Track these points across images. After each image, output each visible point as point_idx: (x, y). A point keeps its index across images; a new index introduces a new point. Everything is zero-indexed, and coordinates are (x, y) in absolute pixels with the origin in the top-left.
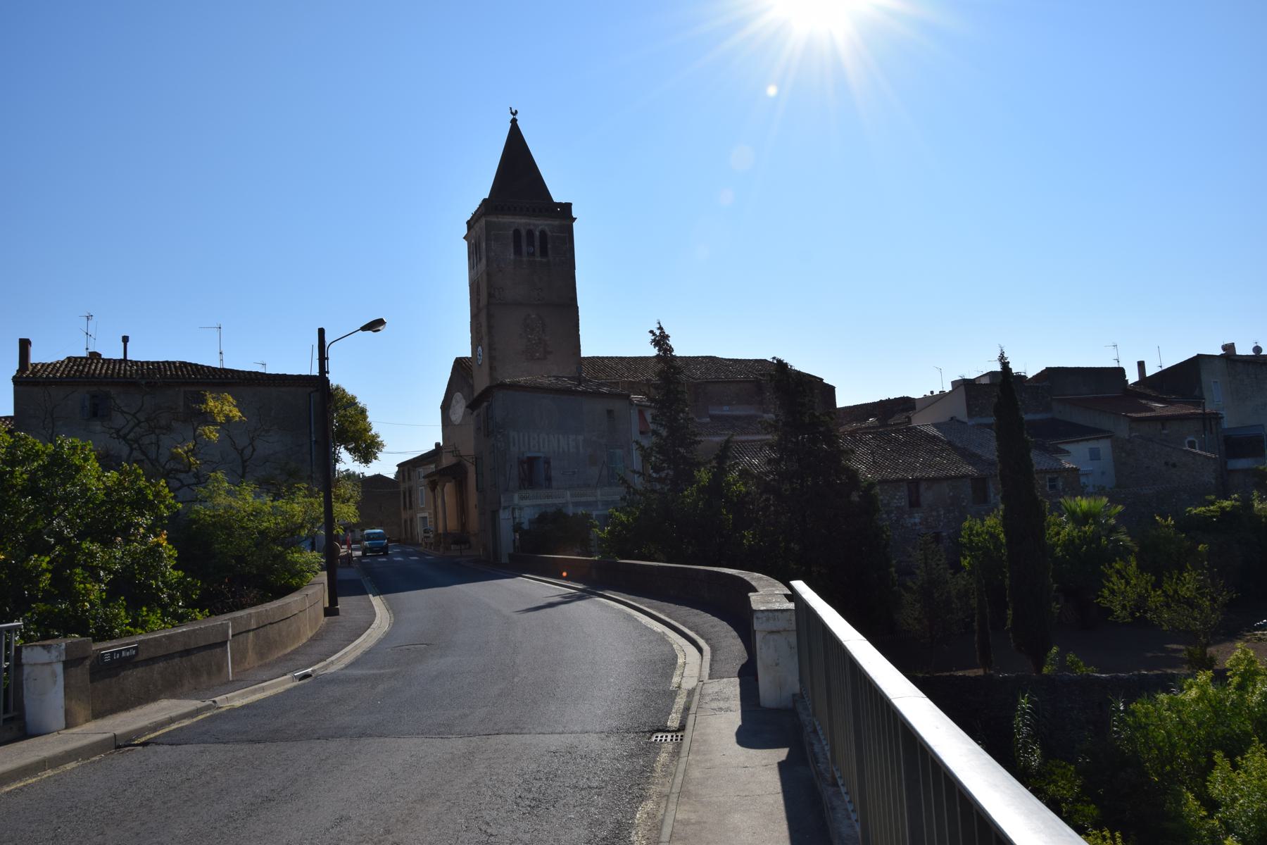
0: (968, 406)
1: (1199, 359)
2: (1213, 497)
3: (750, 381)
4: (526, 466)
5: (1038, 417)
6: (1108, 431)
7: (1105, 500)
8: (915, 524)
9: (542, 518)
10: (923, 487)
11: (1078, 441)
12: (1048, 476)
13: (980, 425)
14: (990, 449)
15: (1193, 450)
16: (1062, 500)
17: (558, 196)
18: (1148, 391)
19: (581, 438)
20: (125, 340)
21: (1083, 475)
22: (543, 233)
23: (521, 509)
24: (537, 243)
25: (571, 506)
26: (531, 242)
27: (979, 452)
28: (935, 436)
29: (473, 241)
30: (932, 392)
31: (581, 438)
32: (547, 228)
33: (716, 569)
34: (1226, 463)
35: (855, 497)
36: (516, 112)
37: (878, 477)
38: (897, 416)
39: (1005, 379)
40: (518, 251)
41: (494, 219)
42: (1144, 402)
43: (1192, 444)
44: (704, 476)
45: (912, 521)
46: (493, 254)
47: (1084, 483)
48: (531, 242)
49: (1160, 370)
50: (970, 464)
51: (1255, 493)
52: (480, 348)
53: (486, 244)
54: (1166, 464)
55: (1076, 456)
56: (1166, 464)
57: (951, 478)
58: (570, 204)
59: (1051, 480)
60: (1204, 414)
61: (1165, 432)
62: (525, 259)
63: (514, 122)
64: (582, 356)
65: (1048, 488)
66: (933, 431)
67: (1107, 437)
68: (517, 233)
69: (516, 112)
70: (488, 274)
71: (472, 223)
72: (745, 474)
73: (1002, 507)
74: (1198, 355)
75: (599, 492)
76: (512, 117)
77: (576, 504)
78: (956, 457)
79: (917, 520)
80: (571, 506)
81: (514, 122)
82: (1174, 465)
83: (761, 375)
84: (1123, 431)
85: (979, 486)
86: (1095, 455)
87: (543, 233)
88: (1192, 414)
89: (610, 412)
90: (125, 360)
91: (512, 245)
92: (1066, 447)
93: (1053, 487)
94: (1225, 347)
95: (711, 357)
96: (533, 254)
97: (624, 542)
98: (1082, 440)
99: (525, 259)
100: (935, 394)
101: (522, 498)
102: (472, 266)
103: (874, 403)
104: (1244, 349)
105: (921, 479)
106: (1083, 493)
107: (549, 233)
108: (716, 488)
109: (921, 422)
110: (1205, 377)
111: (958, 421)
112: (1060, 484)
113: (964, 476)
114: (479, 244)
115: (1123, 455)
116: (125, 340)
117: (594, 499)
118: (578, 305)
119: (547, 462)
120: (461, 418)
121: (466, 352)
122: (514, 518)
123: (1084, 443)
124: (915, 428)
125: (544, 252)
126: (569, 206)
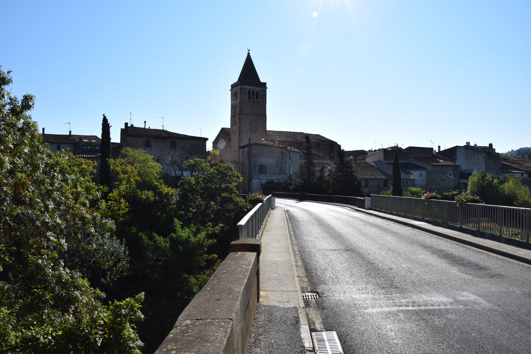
0: (384, 157)
1: (457, 147)
2: (451, 190)
3: (316, 143)
4: (261, 167)
5: (405, 162)
6: (425, 168)
7: (420, 189)
8: (366, 191)
9: (268, 182)
10: (370, 180)
11: (416, 171)
12: (406, 181)
13: (387, 163)
14: (390, 171)
15: (450, 177)
16: (408, 188)
17: (262, 80)
18: (440, 156)
19: (274, 160)
20: (145, 122)
21: (416, 181)
22: (257, 92)
23: (262, 179)
24: (255, 95)
25: (275, 179)
26: (253, 95)
27: (386, 172)
28: (373, 166)
29: (234, 92)
30: (372, 149)
31: (274, 160)
32: (258, 91)
34: (460, 180)
35: (356, 183)
36: (249, 50)
38: (360, 157)
39: (396, 150)
40: (249, 97)
41: (243, 87)
42: (438, 159)
43: (450, 175)
45: (366, 191)
46: (242, 98)
47: (416, 183)
48: (253, 95)
49: (445, 149)
50: (383, 175)
51: (463, 190)
52: (235, 127)
54: (441, 179)
55: (415, 175)
56: (441, 179)
57: (378, 179)
58: (266, 83)
59: (406, 182)
60: (455, 165)
61: (442, 170)
62: (251, 100)
63: (249, 53)
64: (267, 130)
65: (405, 184)
66: (373, 164)
67: (425, 170)
68: (249, 91)
69: (249, 50)
70: (240, 104)
71: (233, 85)
73: (392, 188)
74: (457, 146)
75: (281, 176)
76: (248, 52)
77: (276, 179)
78: (379, 173)
79: (367, 190)
80: (275, 179)
81: (249, 53)
82: (443, 180)
84: (430, 168)
85: (386, 183)
86: (421, 175)
87: (257, 92)
88: (451, 165)
89: (282, 152)
90: (145, 128)
91: (248, 95)
93: (407, 184)
94: (467, 143)
96: (254, 99)
97: (295, 190)
98: (417, 170)
99: (251, 100)
100: (372, 150)
101: (263, 176)
103: (352, 151)
104: (472, 144)
105: (369, 178)
106: (415, 186)
107: (259, 92)
108: (321, 178)
109: (369, 160)
110: (458, 153)
111: (381, 161)
112: (409, 183)
113: (382, 179)
115: (429, 176)
116: (145, 122)
117: (280, 178)
118: (267, 116)
119: (266, 166)
120: (223, 148)
121: (228, 125)
124: (367, 162)
125: (257, 98)
126: (265, 83)
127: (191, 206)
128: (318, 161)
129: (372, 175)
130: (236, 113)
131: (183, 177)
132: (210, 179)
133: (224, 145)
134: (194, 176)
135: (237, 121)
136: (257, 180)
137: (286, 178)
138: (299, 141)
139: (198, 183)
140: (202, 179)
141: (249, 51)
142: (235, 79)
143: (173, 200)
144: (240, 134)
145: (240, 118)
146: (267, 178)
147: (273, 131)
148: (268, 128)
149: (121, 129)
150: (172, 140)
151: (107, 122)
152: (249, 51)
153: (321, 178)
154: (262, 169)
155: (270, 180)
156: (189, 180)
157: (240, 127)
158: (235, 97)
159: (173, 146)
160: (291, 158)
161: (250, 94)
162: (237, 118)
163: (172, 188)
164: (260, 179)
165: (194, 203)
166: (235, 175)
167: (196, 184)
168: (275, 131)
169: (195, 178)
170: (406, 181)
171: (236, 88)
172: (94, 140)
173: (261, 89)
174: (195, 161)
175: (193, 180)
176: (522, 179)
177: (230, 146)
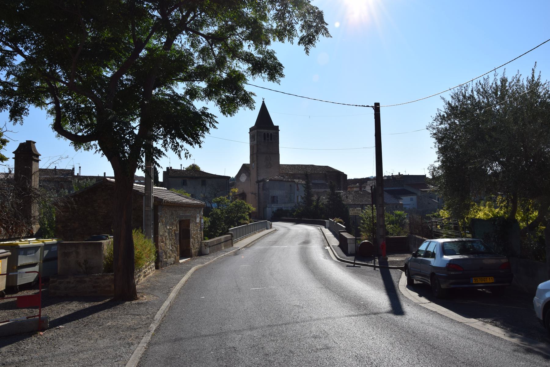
9: (278, 210)
12: (395, 205)
15: (435, 201)
16: (394, 211)
19: (284, 191)
20: (181, 165)
22: (271, 134)
32: (272, 133)
33: (97, 242)
37: (353, 203)
40: (265, 139)
41: (259, 130)
44: (315, 203)
48: (268, 137)
52: (253, 164)
53: (257, 137)
56: (428, 203)
63: (263, 101)
65: (395, 208)
68: (264, 134)
70: (257, 145)
72: (323, 204)
75: (289, 205)
76: (263, 100)
77: (285, 207)
81: (263, 101)
82: (430, 204)
83: (327, 172)
84: (419, 194)
86: (412, 200)
87: (271, 134)
89: (290, 185)
92: (402, 198)
95: (312, 165)
96: (268, 140)
99: (266, 141)
102: (251, 141)
107: (273, 134)
108: (317, 207)
112: (398, 207)
114: (254, 137)
119: (277, 197)
121: (248, 161)
122: (272, 210)
123: (409, 196)
125: (271, 139)
126: (278, 127)
127: (218, 229)
128: (325, 190)
129: (367, 201)
130: (254, 153)
131: (212, 210)
132: (229, 212)
133: (246, 179)
134: (220, 209)
135: (255, 159)
136: (269, 209)
137: (293, 206)
138: (309, 173)
139: (222, 213)
140: (225, 211)
141: (264, 99)
142: (253, 124)
143: (206, 225)
144: (257, 170)
145: (257, 156)
146: (278, 206)
147: (287, 165)
148: (281, 163)
149: (164, 171)
150: (202, 179)
151: (157, 170)
152: (264, 99)
153: (317, 207)
154: (274, 200)
155: (280, 208)
156: (217, 212)
157: (257, 164)
158: (253, 139)
159: (204, 183)
160: (299, 189)
161: (265, 136)
162: (255, 156)
163: (205, 217)
164: (272, 208)
165: (220, 227)
166: (246, 208)
167: (221, 214)
168: (289, 165)
169: (221, 210)
170: (395, 205)
171: (254, 131)
172: (142, 180)
173: (275, 131)
174: (220, 199)
175: (219, 211)
176: (47, 246)
177: (250, 180)
